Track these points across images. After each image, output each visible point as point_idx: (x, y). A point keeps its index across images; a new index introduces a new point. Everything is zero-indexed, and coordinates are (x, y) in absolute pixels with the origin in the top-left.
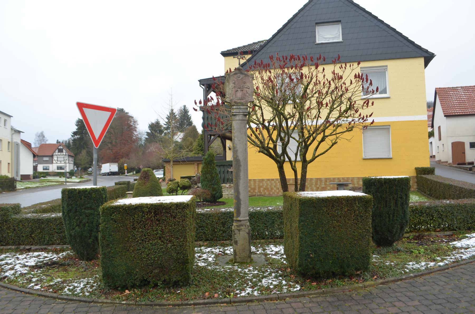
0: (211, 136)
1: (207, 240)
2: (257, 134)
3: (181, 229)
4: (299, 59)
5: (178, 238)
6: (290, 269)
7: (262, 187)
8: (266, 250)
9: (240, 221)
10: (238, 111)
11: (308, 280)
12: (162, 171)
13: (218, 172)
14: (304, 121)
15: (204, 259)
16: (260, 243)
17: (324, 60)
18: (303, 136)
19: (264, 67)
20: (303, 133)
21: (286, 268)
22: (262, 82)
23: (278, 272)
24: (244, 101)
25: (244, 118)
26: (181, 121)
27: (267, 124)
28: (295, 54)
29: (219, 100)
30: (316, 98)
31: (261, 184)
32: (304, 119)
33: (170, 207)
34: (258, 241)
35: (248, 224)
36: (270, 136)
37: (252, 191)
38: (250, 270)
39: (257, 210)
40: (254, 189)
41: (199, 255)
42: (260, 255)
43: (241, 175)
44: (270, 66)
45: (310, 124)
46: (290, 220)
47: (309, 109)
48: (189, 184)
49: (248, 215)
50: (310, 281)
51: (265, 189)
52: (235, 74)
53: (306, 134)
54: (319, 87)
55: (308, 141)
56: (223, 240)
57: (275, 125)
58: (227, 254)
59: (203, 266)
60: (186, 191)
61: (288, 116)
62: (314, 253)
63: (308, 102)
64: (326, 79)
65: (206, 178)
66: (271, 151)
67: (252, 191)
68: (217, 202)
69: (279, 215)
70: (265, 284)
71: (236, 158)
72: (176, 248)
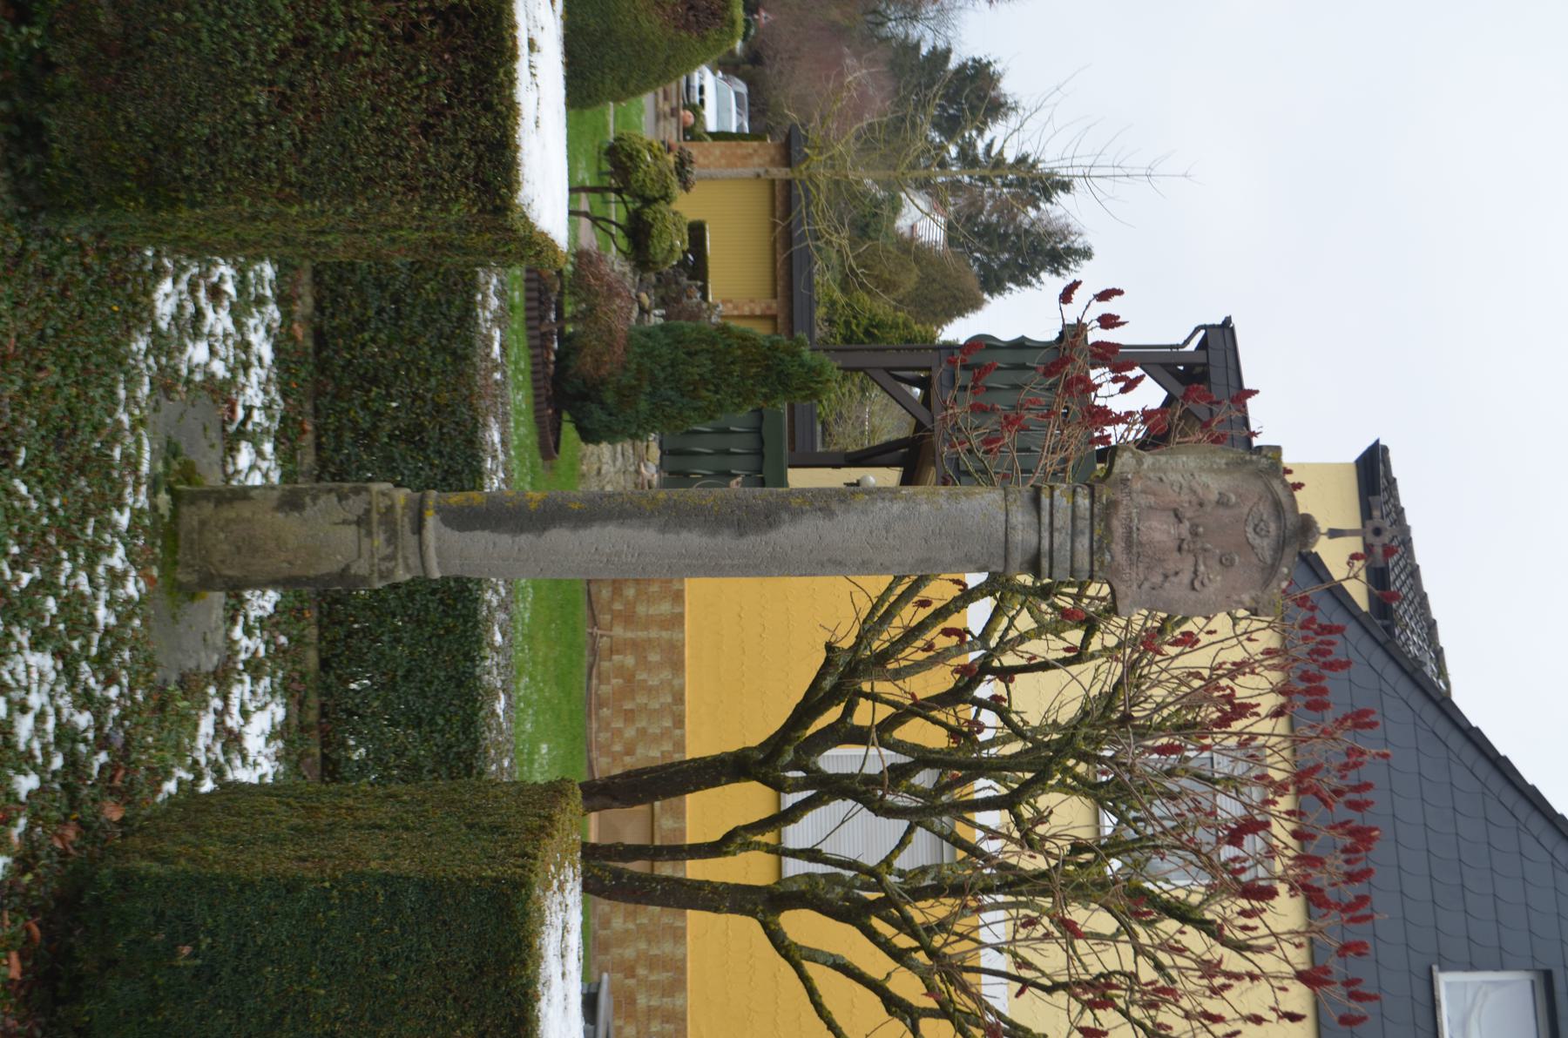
0: (924, 384)
1: (319, 337)
2: (928, 636)
3: (356, 169)
4: (1351, 878)
5: (301, 147)
6: (116, 816)
7: (642, 661)
8: (255, 680)
9: (419, 527)
10: (1063, 519)
11: (35, 930)
12: (740, 126)
13: (722, 420)
14: (1000, 898)
15: (199, 314)
16: (298, 641)
17: (1346, 1020)
18: (918, 894)
19: (1305, 677)
20: (936, 892)
21: (126, 795)
22: (1220, 666)
23: (101, 747)
24: (1121, 558)
25: (1017, 558)
26: (1006, 236)
27: (984, 691)
28: (1379, 854)
29: (1121, 427)
30: (1129, 967)
31: (654, 657)
32: (1010, 899)
33: (488, 107)
34: (312, 633)
35: (402, 576)
36: (921, 708)
37: (618, 606)
38: (116, 579)
39: (488, 630)
40: (629, 619)
41: (229, 288)
42: (219, 640)
43: (684, 534)
44: (1312, 714)
45: (985, 935)
46: (410, 819)
47: (1070, 930)
48: (659, 257)
49: (455, 570)
50: (29, 939)
51: (629, 678)
52: (1277, 506)
53: (925, 912)
54: (1191, 987)
55: (889, 920)
56: (320, 431)
57: (982, 737)
58: (232, 450)
59: (151, 309)
60: (623, 243)
61: (1026, 812)
62: (198, 969)
63: (1104, 922)
64: (1239, 1026)
65: (689, 354)
66: (833, 714)
67: (618, 606)
68: (558, 413)
69: (459, 756)
70: (21, 668)
71: (787, 508)
72: (244, 134)
